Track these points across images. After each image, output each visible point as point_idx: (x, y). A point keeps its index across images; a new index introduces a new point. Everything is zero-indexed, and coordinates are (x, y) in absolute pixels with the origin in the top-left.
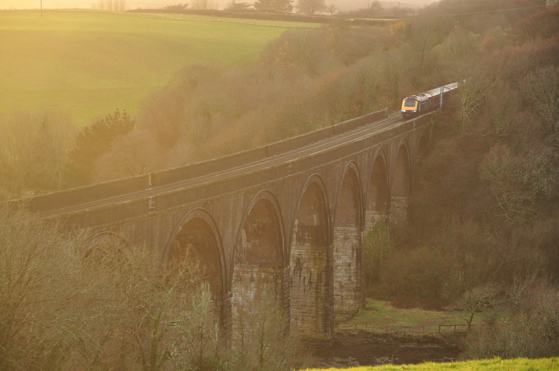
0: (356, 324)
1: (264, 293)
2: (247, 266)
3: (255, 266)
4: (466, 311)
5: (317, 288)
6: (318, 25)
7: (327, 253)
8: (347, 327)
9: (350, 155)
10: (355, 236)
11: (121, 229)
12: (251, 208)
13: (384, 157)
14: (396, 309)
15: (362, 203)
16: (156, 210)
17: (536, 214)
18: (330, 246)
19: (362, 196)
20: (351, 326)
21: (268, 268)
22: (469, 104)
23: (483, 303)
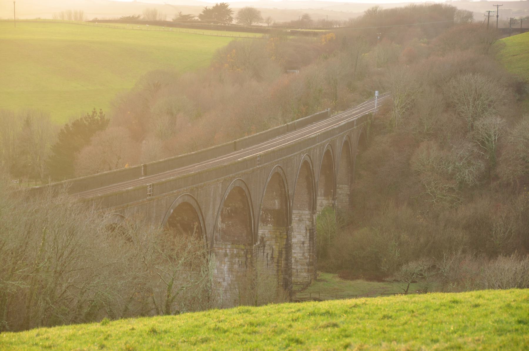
0: (311, 293)
1: (236, 266)
2: (222, 244)
3: (229, 243)
4: (404, 281)
5: (278, 263)
6: (259, 35)
7: (287, 232)
8: (302, 295)
9: (305, 149)
10: (308, 218)
11: (126, 211)
12: (228, 194)
13: (331, 151)
14: (343, 281)
15: (314, 190)
16: (153, 196)
17: (459, 200)
18: (289, 227)
19: (315, 184)
20: (306, 295)
21: (239, 245)
22: (400, 106)
23: (418, 275)
